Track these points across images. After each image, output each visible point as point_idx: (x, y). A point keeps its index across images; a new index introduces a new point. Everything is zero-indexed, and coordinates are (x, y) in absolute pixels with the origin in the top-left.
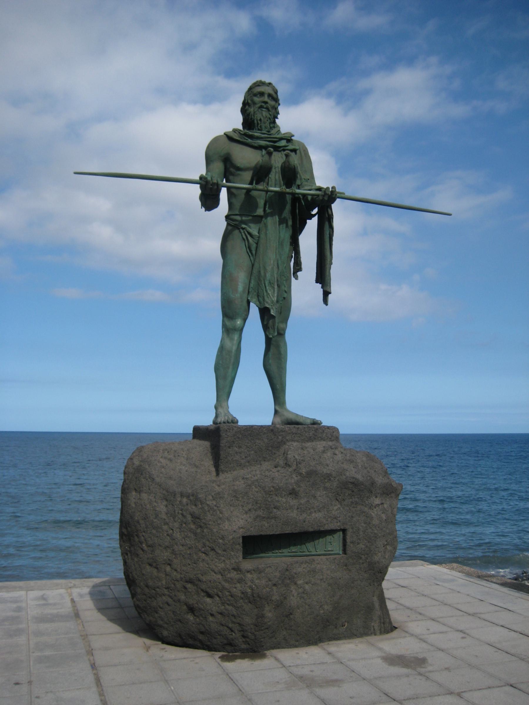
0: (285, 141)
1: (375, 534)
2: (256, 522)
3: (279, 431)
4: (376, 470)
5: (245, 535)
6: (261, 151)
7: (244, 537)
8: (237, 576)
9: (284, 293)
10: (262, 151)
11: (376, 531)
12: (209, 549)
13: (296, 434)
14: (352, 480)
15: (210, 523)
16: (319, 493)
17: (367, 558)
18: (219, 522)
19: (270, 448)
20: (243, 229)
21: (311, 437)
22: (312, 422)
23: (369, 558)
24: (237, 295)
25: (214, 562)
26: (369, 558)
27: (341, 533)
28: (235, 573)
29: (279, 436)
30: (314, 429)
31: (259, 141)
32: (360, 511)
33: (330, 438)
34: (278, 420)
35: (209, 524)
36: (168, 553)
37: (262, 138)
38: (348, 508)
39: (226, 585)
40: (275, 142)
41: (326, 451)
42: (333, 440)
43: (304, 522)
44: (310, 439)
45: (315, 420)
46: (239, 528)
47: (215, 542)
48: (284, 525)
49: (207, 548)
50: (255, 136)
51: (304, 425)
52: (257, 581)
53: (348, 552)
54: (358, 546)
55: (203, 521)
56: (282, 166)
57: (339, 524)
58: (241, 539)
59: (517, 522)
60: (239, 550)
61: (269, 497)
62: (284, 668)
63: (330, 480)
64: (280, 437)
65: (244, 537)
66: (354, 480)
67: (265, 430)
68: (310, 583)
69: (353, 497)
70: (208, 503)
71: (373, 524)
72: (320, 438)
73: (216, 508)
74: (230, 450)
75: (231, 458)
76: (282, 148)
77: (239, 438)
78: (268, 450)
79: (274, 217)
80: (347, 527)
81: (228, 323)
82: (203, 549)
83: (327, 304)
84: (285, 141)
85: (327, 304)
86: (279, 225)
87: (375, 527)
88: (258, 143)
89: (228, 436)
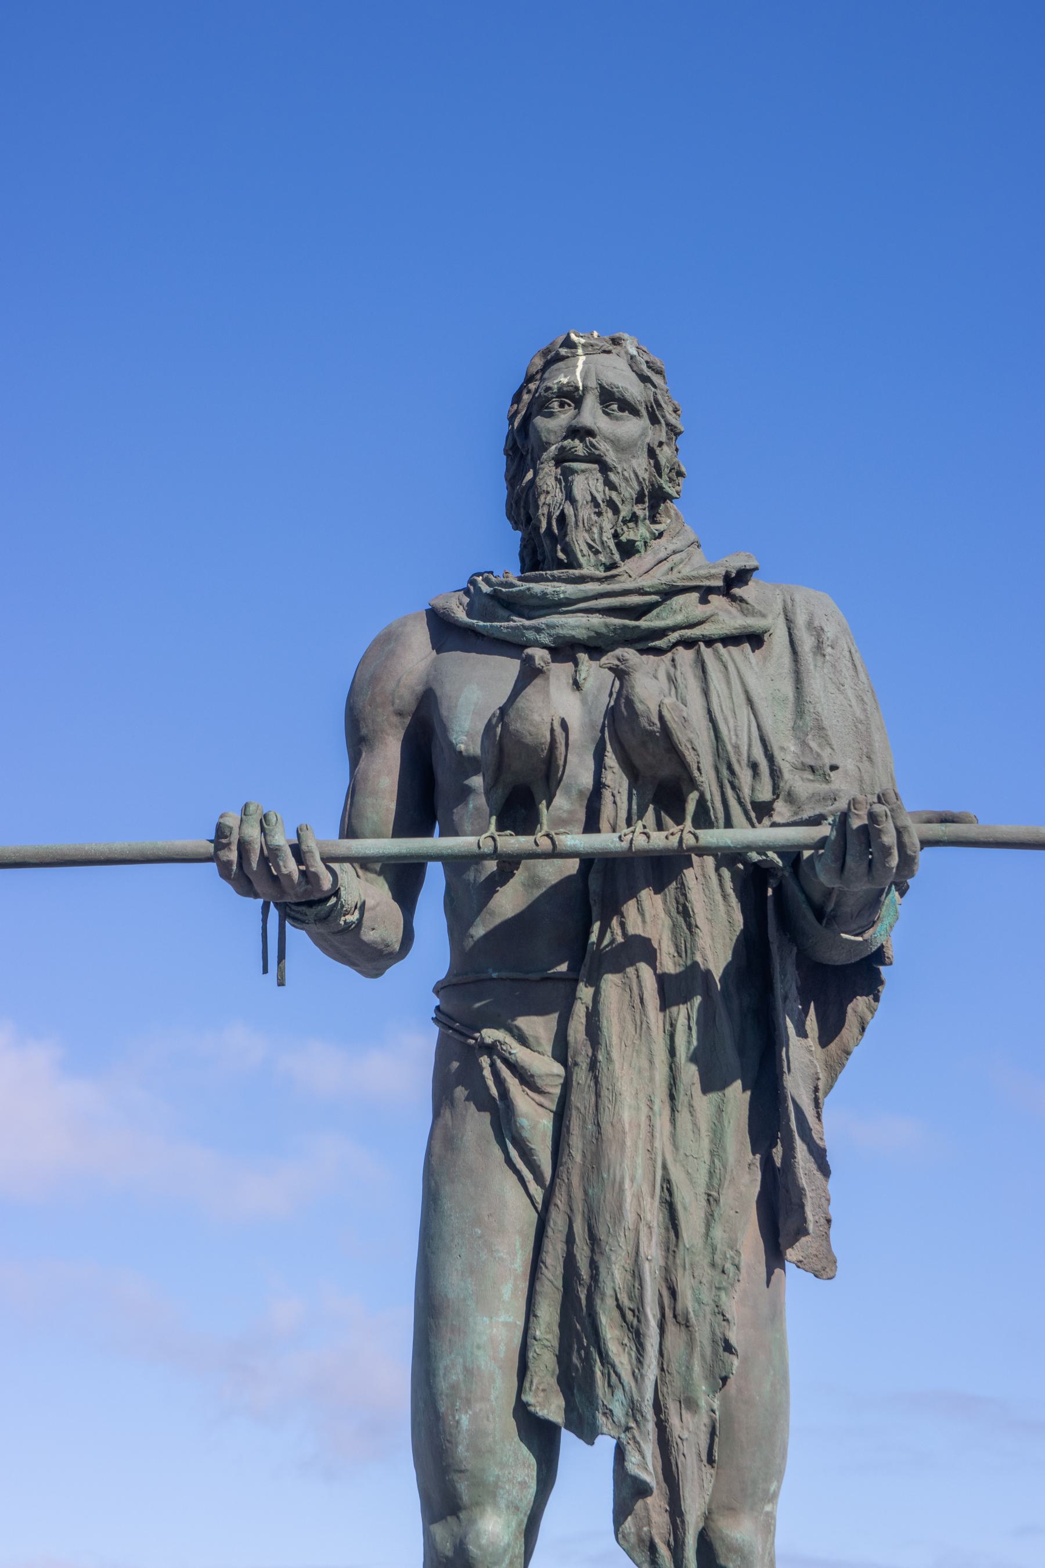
50: (534, 596)
76: (674, 637)
79: (630, 970)
88: (550, 626)
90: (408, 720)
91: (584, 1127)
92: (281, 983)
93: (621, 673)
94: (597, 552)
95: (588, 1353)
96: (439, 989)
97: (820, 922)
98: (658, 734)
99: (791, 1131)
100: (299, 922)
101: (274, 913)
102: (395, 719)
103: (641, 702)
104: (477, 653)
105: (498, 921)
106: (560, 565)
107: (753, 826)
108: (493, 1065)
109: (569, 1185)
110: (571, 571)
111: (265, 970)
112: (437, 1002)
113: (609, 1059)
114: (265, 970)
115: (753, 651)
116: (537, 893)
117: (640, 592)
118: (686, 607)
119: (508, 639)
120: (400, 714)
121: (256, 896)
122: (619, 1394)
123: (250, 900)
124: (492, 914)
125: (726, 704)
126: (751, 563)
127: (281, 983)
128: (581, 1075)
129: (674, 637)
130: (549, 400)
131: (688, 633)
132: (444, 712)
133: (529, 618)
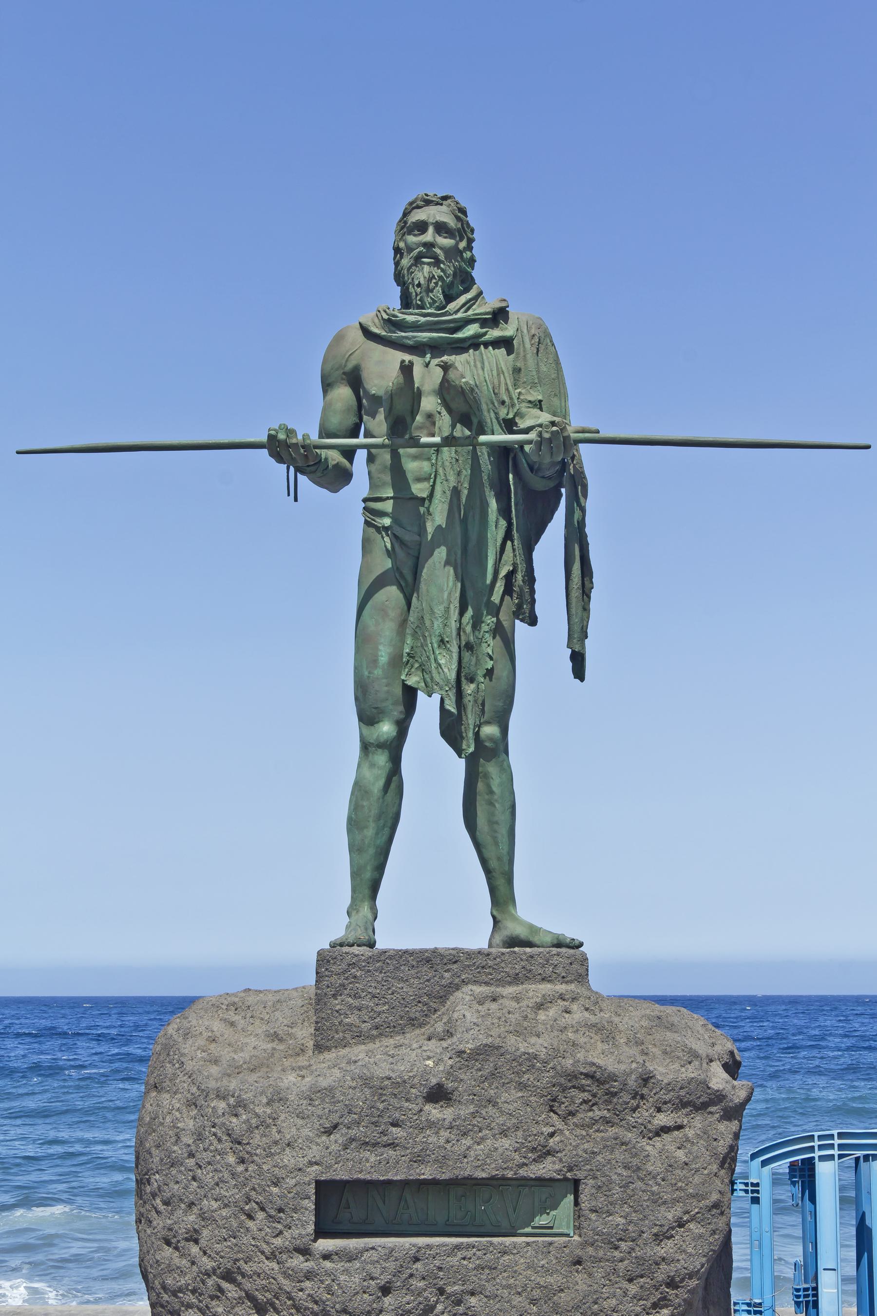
1: (653, 1193)
2: (348, 1151)
3: (445, 961)
4: (668, 1049)
5: (322, 1179)
7: (318, 1183)
8: (306, 1264)
9: (488, 659)
11: (655, 1188)
12: (256, 1206)
13: (483, 967)
15: (258, 1151)
16: (505, 1096)
17: (633, 1249)
18: (272, 1151)
19: (425, 999)
21: (517, 974)
22: (555, 942)
23: (637, 1249)
24: (376, 672)
25: (263, 1233)
26: (637, 1249)
28: (301, 1258)
29: (445, 971)
30: (524, 957)
32: (616, 1139)
33: (563, 977)
34: (498, 939)
35: (256, 1155)
36: (194, 1216)
38: (584, 1133)
39: (287, 1285)
41: (549, 1004)
42: (571, 982)
43: (465, 1157)
44: (516, 979)
45: (561, 937)
46: (311, 1164)
47: (264, 1190)
48: (415, 1162)
49: (254, 1204)
51: (538, 947)
52: (342, 1278)
54: (610, 1218)
55: (248, 1148)
58: (313, 1185)
59: (127, 1067)
60: (307, 1210)
61: (379, 1099)
63: (533, 1066)
64: (447, 975)
65: (318, 1183)
66: (594, 1069)
67: (413, 960)
68: (481, 1293)
69: (594, 1108)
70: (257, 1111)
71: (647, 1171)
72: (539, 977)
73: (271, 1121)
74: (337, 1002)
75: (339, 1020)
77: (355, 977)
78: (420, 1002)
81: (366, 731)
82: (247, 1207)
83: (582, 679)
85: (582, 679)
87: (654, 1178)
88: (415, 337)
89: (332, 972)
92: (296, 500)
93: (446, 367)
97: (532, 473)
98: (424, 250)
99: (438, 320)
100: (303, 473)
101: (292, 469)
103: (453, 382)
104: (550, 522)
107: (365, 500)
110: (423, 311)
111: (289, 495)
114: (289, 495)
115: (494, 350)
119: (395, 341)
121: (284, 463)
127: (296, 500)
133: (405, 332)
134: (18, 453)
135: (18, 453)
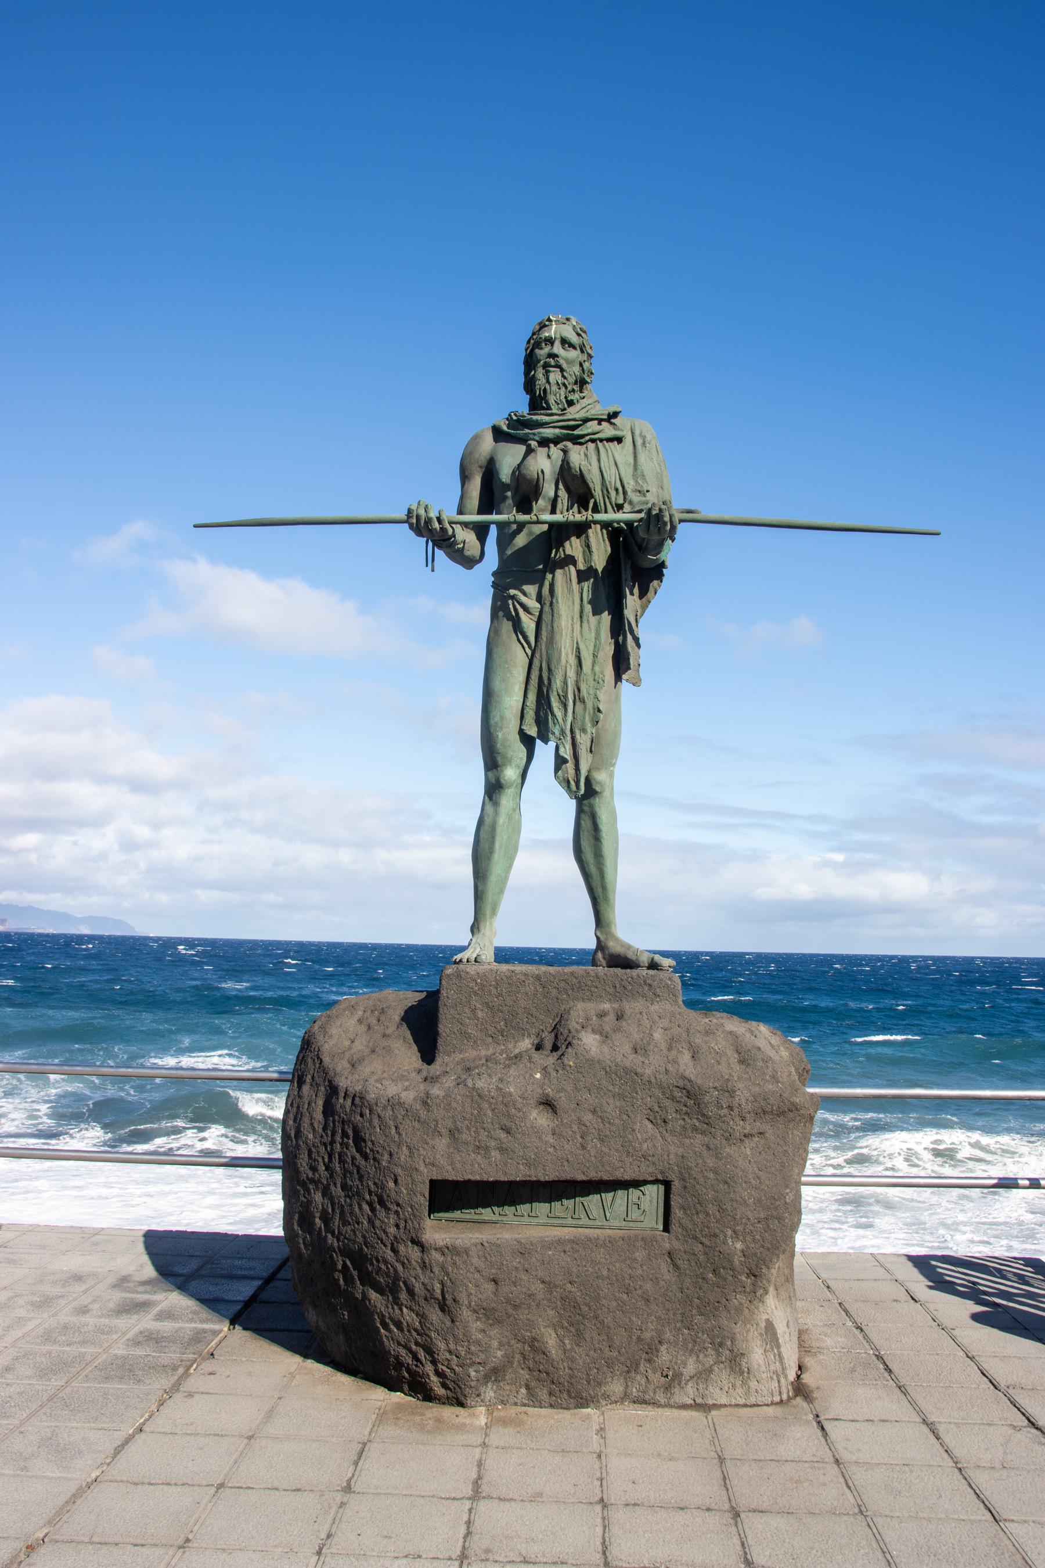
0: (596, 422)
6: (547, 449)
7: (432, 1182)
10: (549, 448)
14: (681, 1084)
20: (513, 597)
27: (662, 1188)
31: (541, 430)
37: (547, 423)
40: (577, 427)
50: (533, 421)
53: (674, 1227)
56: (513, 472)
57: (651, 1170)
62: (860, 1517)
65: (432, 1182)
76: (587, 438)
79: (566, 568)
80: (671, 1176)
84: (596, 422)
86: (579, 582)
88: (539, 433)
90: (484, 469)
91: (547, 627)
92: (433, 570)
94: (558, 404)
95: (546, 712)
96: (494, 574)
101: (430, 544)
102: (478, 469)
105: (516, 548)
106: (544, 409)
108: (513, 604)
109: (541, 649)
111: (427, 566)
112: (493, 579)
113: (557, 602)
114: (427, 566)
116: (532, 538)
117: (574, 420)
118: (592, 426)
120: (480, 467)
122: (557, 726)
123: (421, 538)
124: (514, 546)
125: (607, 465)
126: (618, 410)
127: (433, 570)
128: (547, 608)
129: (587, 438)
130: (541, 342)
131: (593, 437)
132: (497, 466)
134: (195, 526)
135: (195, 526)
